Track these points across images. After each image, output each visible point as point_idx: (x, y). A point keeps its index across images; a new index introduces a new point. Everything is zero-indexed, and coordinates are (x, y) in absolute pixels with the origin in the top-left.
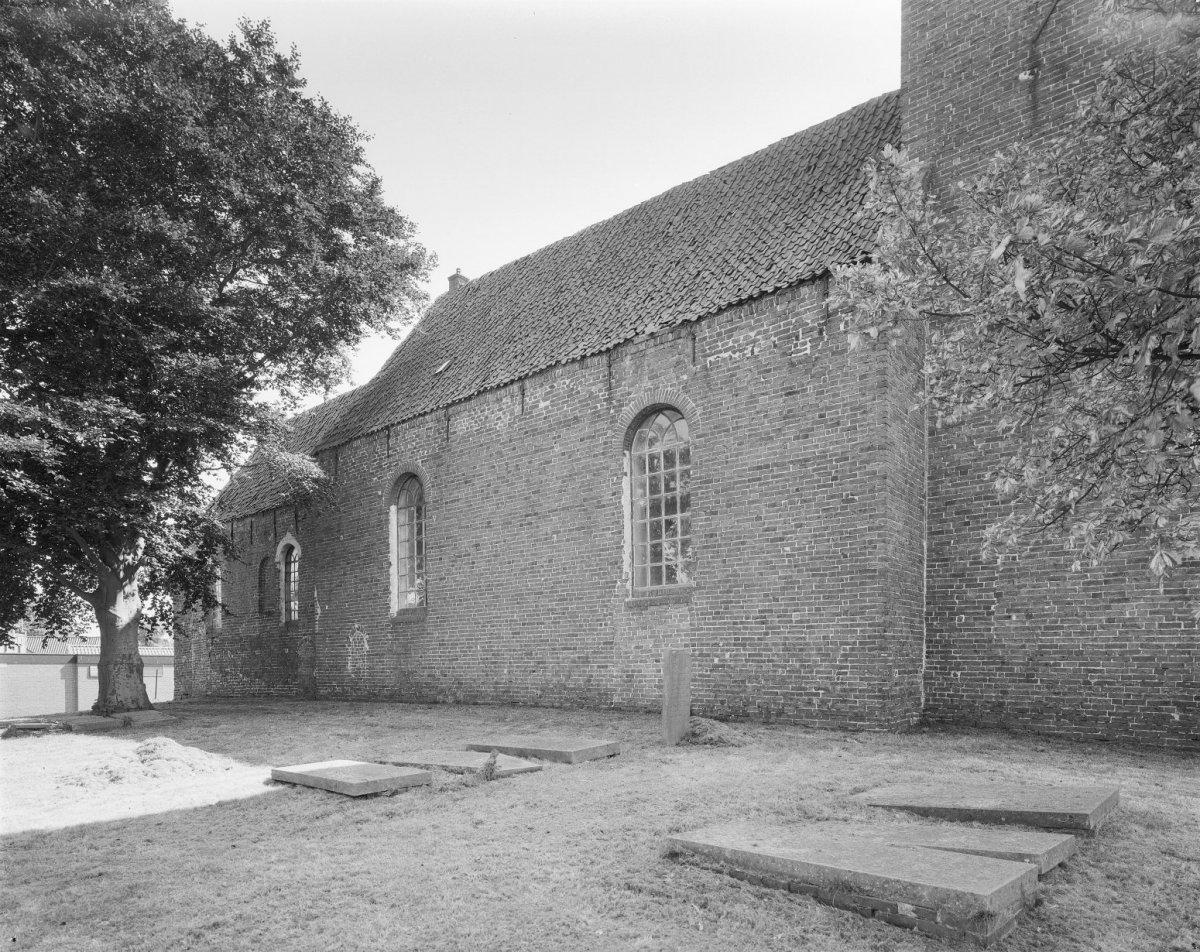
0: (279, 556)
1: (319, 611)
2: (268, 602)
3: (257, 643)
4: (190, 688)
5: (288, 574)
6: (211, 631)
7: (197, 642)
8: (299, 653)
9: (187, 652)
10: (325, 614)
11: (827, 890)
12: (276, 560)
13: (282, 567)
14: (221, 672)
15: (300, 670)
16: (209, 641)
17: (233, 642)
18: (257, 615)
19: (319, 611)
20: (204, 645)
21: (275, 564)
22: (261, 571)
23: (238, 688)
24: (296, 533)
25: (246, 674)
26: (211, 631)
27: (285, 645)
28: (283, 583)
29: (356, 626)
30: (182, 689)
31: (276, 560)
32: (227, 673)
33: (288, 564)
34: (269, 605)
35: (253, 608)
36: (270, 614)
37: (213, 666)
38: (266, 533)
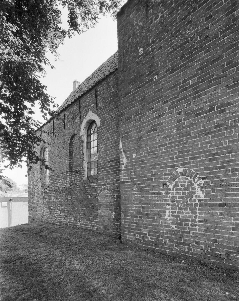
0: (83, 131)
1: (125, 161)
2: (75, 164)
3: (69, 191)
4: (35, 216)
5: (88, 143)
6: (44, 185)
7: (38, 192)
8: (99, 199)
9: (33, 197)
10: (132, 164)
11: (156, 283)
12: (81, 134)
13: (85, 139)
14: (49, 208)
15: (99, 211)
16: (43, 191)
17: (55, 191)
18: (69, 173)
19: (125, 161)
20: (40, 193)
21: (80, 137)
22: (71, 145)
23: (58, 219)
24: (97, 109)
25: (62, 211)
26: (44, 185)
27: (88, 193)
28: (85, 150)
29: (180, 170)
30: (32, 216)
31: (81, 134)
32: (52, 209)
33: (88, 136)
34: (76, 167)
35: (66, 169)
36: (76, 172)
37: (45, 205)
38: (74, 118)
